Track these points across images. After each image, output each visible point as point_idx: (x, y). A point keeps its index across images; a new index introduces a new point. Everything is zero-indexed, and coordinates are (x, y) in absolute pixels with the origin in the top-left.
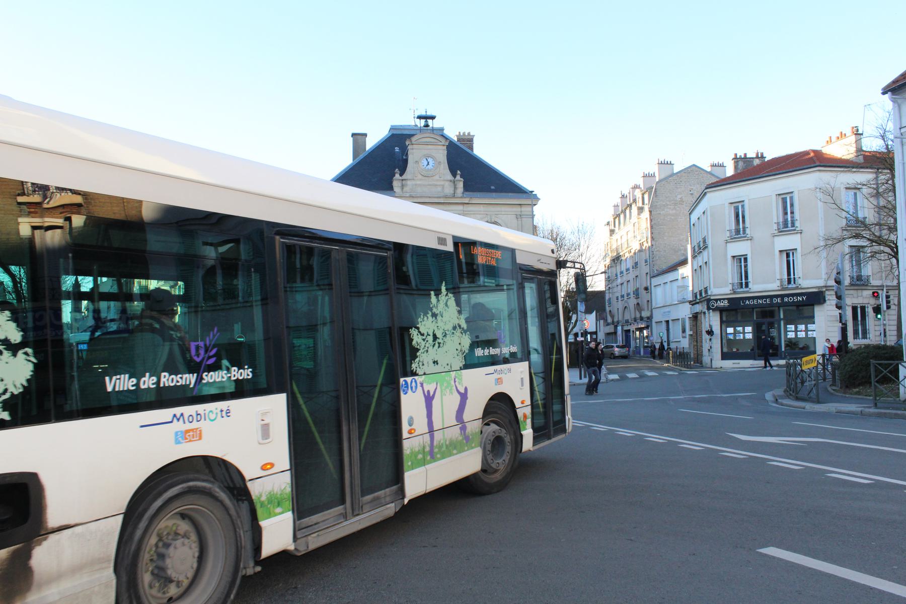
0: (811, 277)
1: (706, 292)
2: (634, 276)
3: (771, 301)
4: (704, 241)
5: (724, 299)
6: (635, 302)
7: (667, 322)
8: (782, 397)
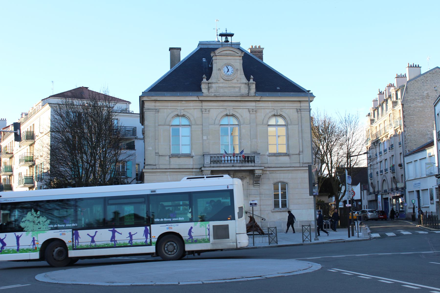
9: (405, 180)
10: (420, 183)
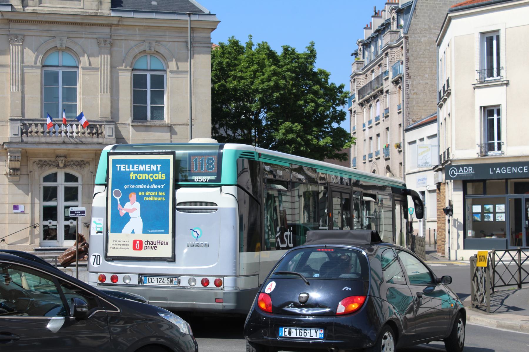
5: (468, 166)
9: (404, 172)
10: (425, 179)
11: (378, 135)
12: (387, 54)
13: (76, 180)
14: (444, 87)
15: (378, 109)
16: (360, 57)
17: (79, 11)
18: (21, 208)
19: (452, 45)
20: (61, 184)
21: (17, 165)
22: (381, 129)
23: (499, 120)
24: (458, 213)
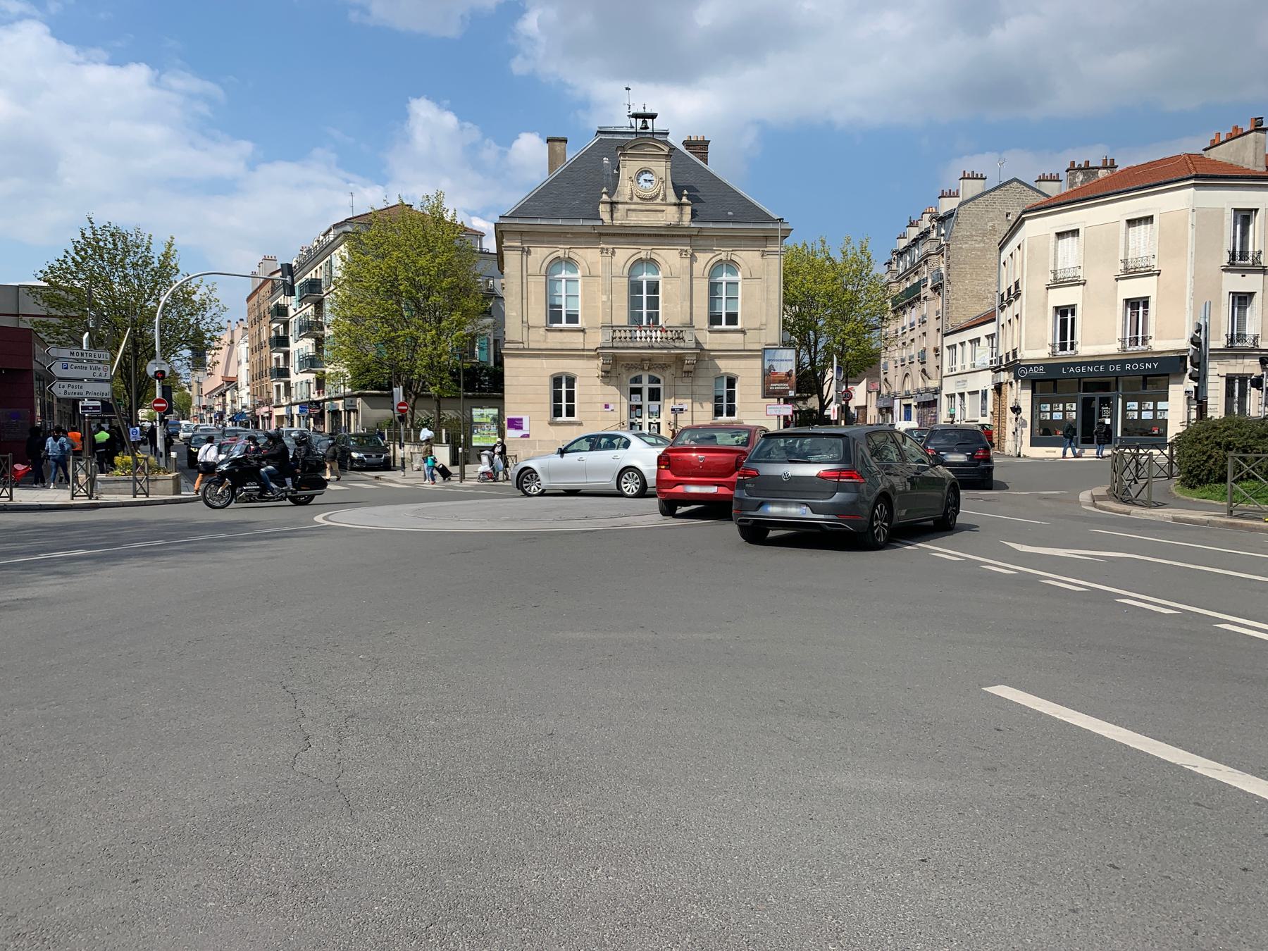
0: (1168, 336)
1: (1015, 355)
2: (920, 333)
3: (1106, 368)
4: (1017, 284)
6: (921, 367)
7: (962, 395)
8: (1101, 498)
11: (913, 340)
12: (926, 262)
13: (658, 381)
14: (1009, 290)
15: (912, 315)
16: (894, 267)
17: (663, 223)
18: (611, 407)
19: (1025, 247)
20: (646, 385)
21: (608, 368)
22: (917, 332)
23: (1073, 320)
24: (1026, 414)
